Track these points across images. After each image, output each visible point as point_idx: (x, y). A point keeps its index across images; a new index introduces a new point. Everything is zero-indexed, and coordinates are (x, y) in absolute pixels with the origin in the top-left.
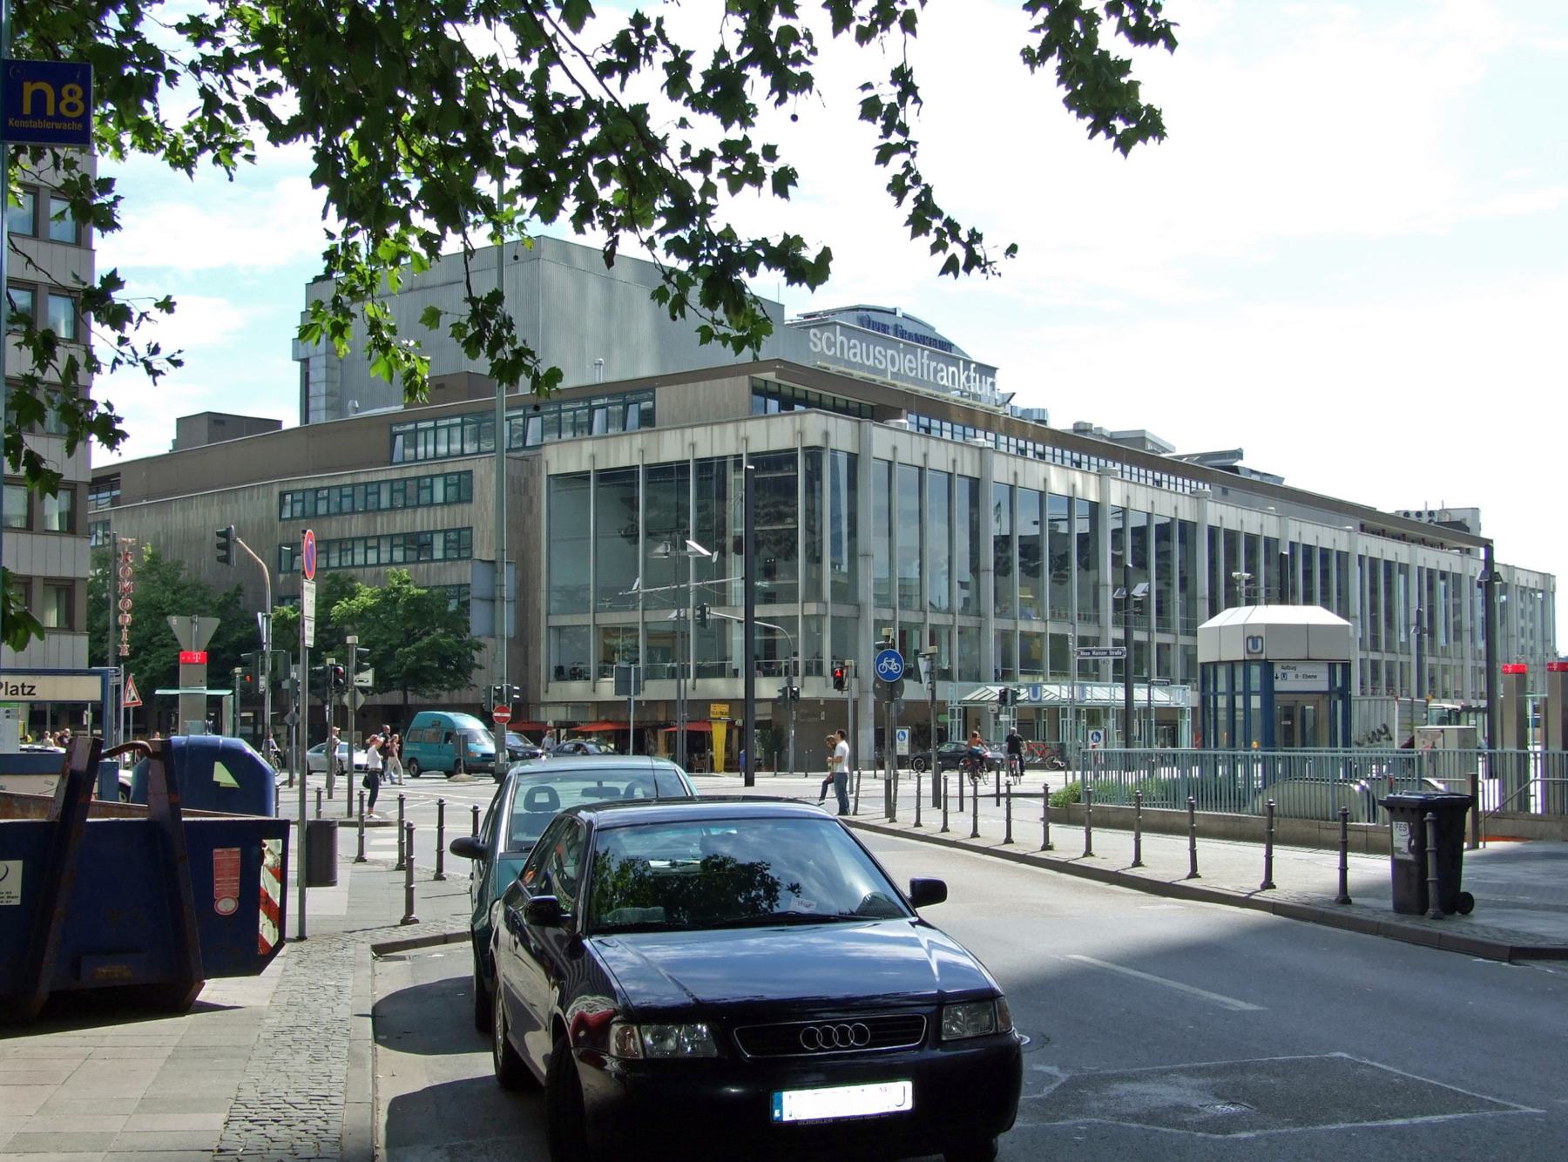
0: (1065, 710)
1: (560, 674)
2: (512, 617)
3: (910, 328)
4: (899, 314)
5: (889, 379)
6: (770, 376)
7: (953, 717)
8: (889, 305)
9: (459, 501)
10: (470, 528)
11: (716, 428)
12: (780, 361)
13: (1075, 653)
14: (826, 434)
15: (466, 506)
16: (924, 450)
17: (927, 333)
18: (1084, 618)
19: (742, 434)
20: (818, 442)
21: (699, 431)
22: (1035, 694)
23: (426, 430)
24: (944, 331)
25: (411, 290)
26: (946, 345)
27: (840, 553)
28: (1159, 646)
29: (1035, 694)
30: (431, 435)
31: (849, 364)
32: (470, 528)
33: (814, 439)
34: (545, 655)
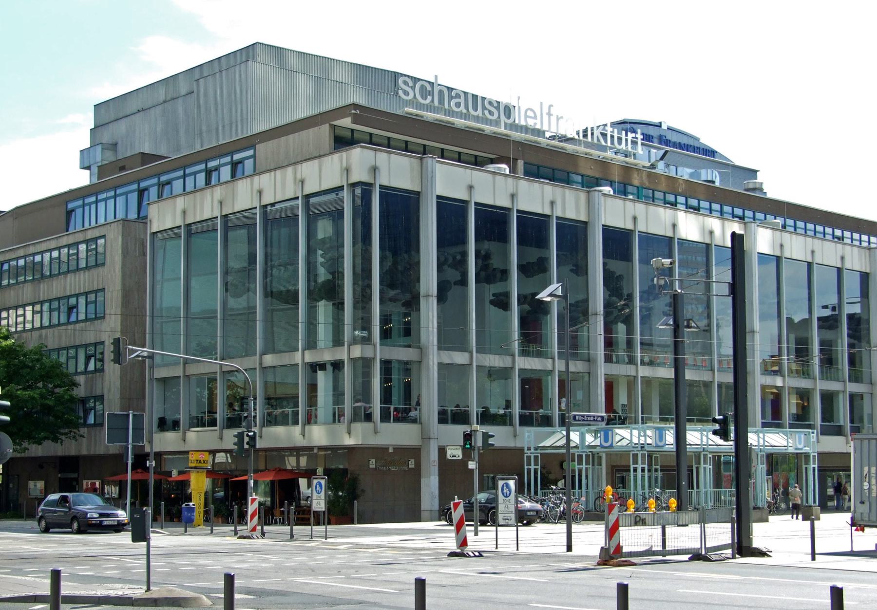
0: (635, 456)
1: (164, 425)
2: (783, 410)
3: (674, 138)
4: (664, 127)
5: (502, 130)
6: (346, 122)
7: (580, 463)
8: (656, 120)
9: (97, 265)
10: (103, 290)
11: (278, 172)
12: (355, 106)
13: (790, 406)
14: (374, 170)
15: (100, 269)
16: (511, 190)
17: (691, 142)
18: (825, 376)
19: (299, 177)
20: (365, 178)
21: (265, 177)
22: (606, 440)
23: (90, 204)
24: (708, 140)
25: (165, 102)
26: (712, 153)
27: (413, 303)
28: (852, 397)
29: (606, 440)
30: (93, 206)
31: (449, 112)
32: (103, 290)
33: (359, 175)
34: (153, 408)
